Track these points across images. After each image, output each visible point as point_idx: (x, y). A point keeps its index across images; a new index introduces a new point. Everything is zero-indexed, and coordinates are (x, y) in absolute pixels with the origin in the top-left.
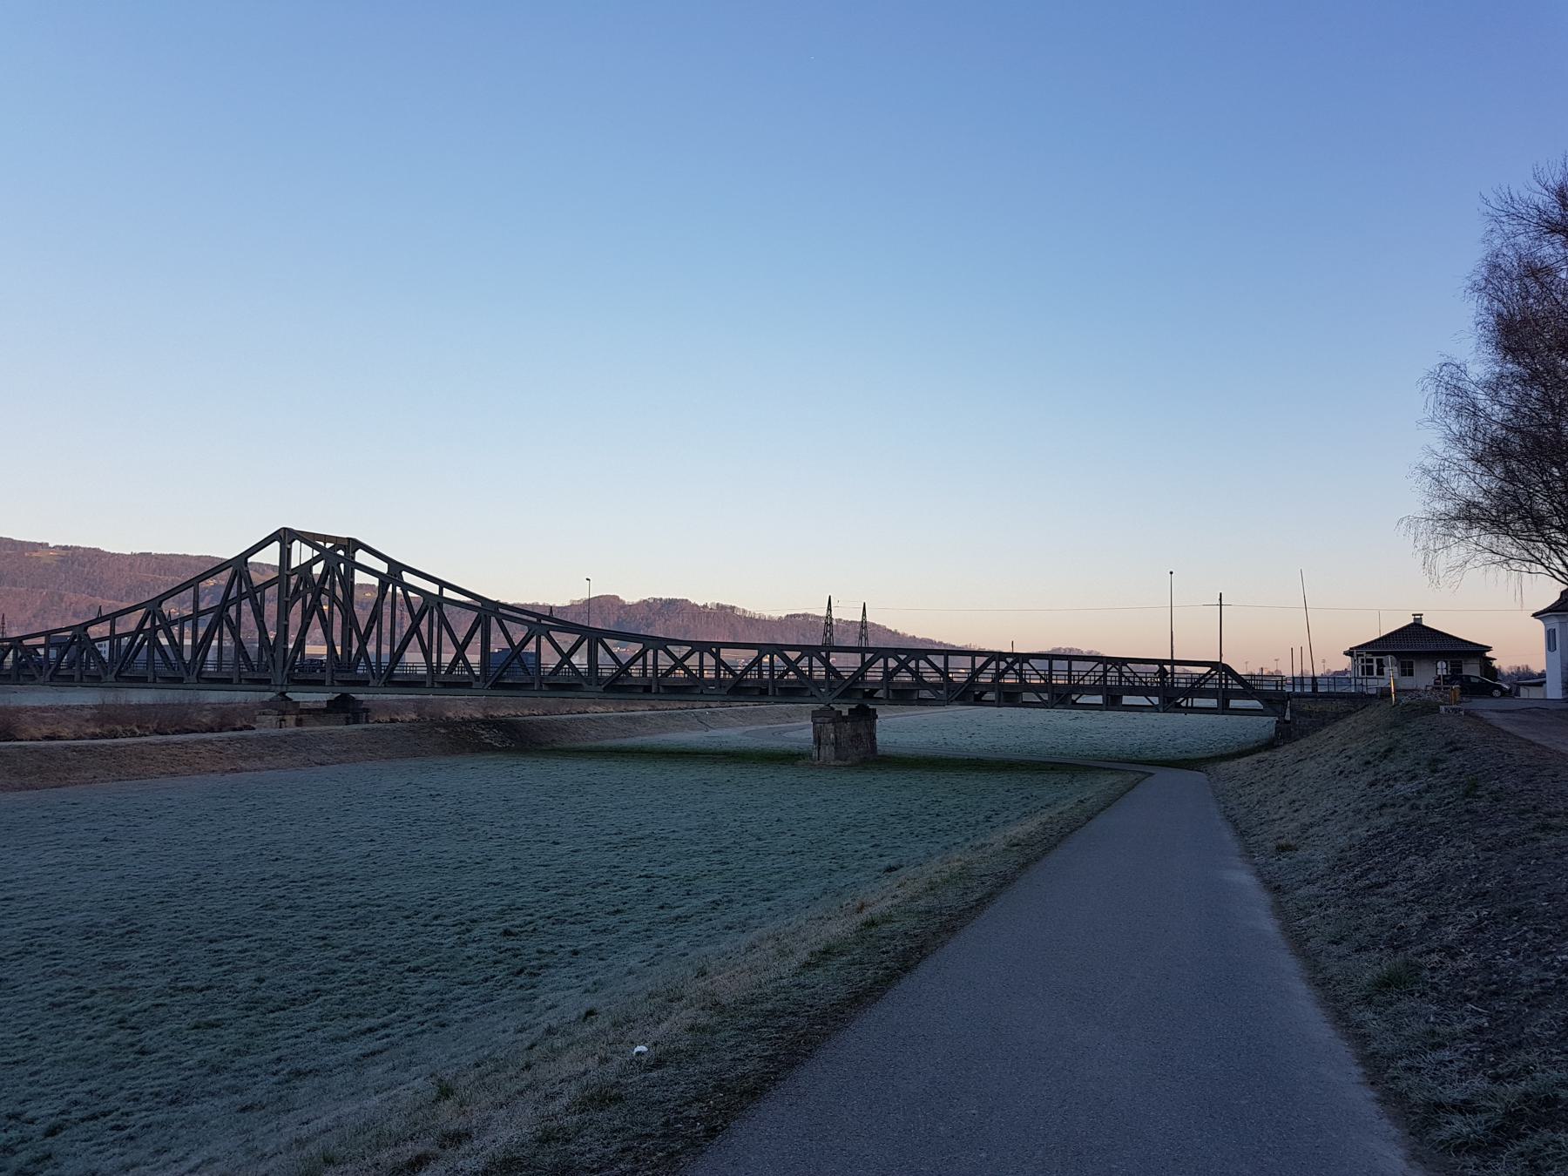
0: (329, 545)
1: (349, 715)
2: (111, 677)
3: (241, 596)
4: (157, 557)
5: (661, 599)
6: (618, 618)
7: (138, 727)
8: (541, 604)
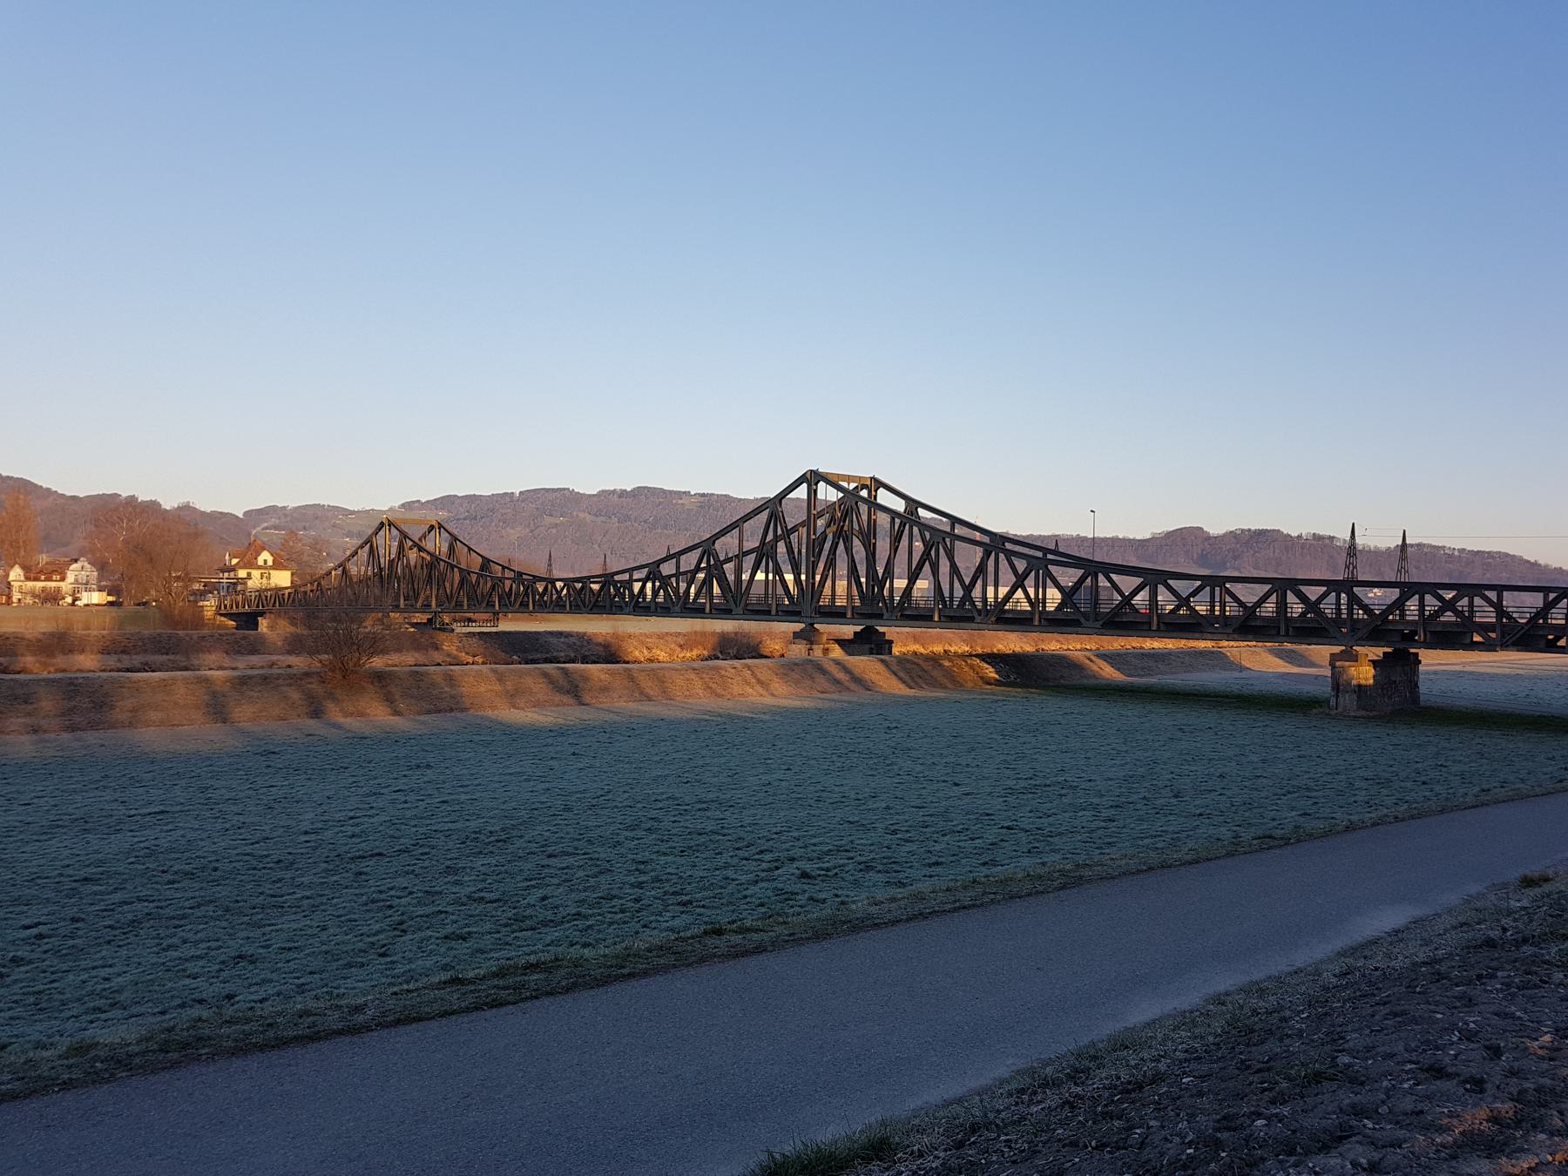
0: (853, 486)
1: (873, 646)
2: (677, 609)
3: (776, 539)
5: (1250, 530)
6: (1202, 551)
7: (721, 652)
8: (1121, 537)
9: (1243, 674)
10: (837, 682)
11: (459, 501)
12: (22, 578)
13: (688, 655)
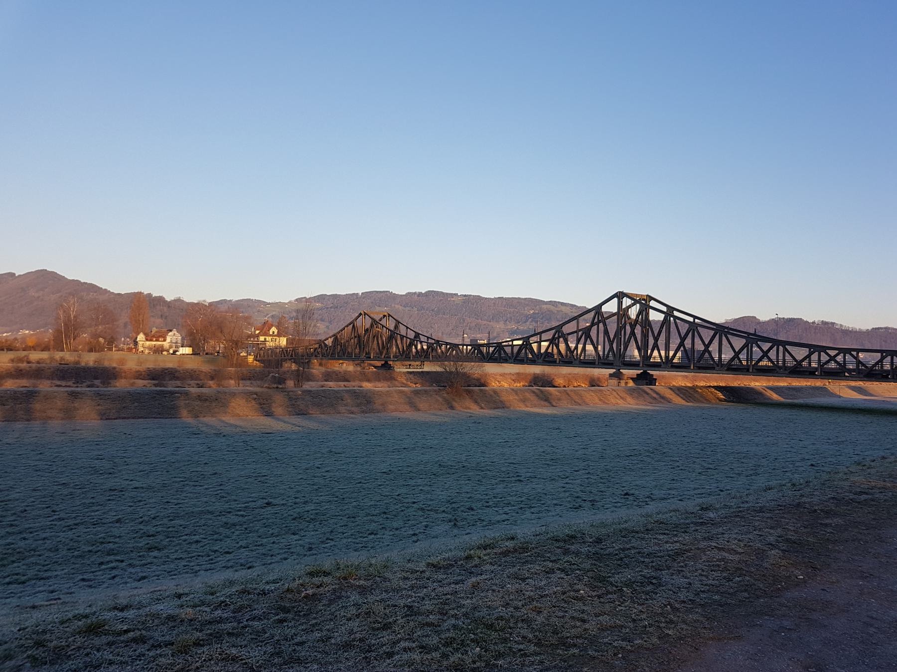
0: (638, 298)
4: (506, 299)
9: (841, 399)
10: (655, 399)
11: (328, 297)
12: (144, 339)
13: (518, 385)
